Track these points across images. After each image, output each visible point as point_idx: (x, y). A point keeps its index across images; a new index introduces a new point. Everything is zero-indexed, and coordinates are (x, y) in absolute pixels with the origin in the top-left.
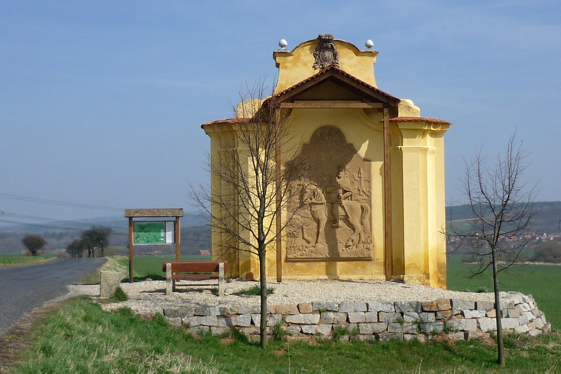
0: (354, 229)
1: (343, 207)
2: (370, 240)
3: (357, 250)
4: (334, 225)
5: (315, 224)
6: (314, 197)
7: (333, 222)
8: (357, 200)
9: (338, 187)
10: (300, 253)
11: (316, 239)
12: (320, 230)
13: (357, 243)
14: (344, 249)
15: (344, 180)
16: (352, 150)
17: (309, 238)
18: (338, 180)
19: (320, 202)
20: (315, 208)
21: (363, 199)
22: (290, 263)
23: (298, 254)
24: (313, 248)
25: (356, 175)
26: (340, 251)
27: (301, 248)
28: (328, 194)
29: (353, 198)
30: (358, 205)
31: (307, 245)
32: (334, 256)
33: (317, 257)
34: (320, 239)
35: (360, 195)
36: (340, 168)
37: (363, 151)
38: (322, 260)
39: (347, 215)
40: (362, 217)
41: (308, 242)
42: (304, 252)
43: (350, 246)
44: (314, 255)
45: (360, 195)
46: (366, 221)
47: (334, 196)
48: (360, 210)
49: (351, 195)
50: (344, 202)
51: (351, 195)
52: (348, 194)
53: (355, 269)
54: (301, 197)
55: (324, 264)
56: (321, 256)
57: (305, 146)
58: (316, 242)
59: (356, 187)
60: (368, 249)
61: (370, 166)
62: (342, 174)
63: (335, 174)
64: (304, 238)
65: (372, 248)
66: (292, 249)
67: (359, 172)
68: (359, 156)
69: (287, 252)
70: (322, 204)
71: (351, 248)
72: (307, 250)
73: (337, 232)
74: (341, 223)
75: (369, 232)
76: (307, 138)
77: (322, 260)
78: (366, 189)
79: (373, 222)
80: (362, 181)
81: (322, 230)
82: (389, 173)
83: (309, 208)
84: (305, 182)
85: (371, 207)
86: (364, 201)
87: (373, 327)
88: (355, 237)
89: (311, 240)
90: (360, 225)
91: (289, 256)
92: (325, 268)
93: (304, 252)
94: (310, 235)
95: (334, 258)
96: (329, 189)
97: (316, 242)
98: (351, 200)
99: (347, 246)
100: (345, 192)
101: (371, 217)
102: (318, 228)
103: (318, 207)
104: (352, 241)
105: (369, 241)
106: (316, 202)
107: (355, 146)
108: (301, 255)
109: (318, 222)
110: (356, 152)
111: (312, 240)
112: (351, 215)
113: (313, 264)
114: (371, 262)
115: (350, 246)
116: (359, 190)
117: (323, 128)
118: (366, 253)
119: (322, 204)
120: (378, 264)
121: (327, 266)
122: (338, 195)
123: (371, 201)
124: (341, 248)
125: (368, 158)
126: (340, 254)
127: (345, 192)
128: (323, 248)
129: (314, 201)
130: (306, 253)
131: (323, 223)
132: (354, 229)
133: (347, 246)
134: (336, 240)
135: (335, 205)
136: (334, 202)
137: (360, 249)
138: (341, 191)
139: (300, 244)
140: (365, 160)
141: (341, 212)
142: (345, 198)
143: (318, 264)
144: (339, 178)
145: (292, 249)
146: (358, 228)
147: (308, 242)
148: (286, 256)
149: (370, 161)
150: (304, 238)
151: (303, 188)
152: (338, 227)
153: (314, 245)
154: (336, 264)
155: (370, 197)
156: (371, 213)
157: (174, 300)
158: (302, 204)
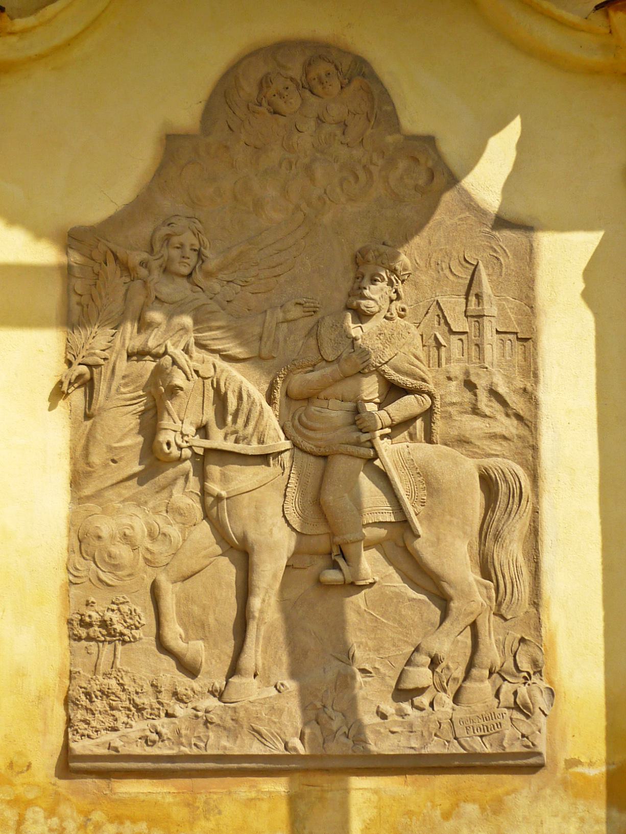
0: (443, 601)
1: (384, 479)
2: (530, 660)
3: (461, 713)
4: (332, 576)
5: (228, 571)
6: (222, 423)
7: (326, 556)
8: (462, 442)
9: (360, 363)
10: (139, 726)
11: (229, 648)
12: (256, 603)
13: (459, 673)
14: (389, 707)
15: (389, 330)
16: (434, 173)
17: (195, 649)
18: (355, 330)
19: (253, 448)
20: (225, 479)
21: (494, 437)
22: (91, 784)
23: (130, 736)
24: (212, 702)
25: (454, 306)
26: (369, 719)
27: (146, 700)
28: (297, 404)
29: (439, 426)
30: (463, 471)
31: (183, 682)
32: (334, 749)
33: (236, 751)
34: (253, 656)
35: (475, 411)
36: (368, 263)
37: (489, 177)
38: (268, 767)
39: (404, 523)
40: (488, 534)
41: (190, 669)
42: (162, 724)
43: (420, 691)
44: (218, 743)
45: (475, 411)
46: (511, 554)
47: (335, 413)
48: (478, 498)
49: (428, 415)
50: (389, 451)
51: (428, 415)
52: (408, 405)
53: (446, 816)
54: (150, 423)
55: (277, 786)
56: (256, 749)
57: (172, 144)
58: (234, 670)
59: (456, 369)
60: (523, 709)
61: (528, 258)
62: (376, 294)
63: (340, 298)
64: (163, 647)
65: (541, 701)
66: (100, 704)
67: (471, 289)
68: (470, 205)
69: (69, 722)
70: (264, 459)
71: (424, 700)
72: (180, 710)
73: (352, 617)
74: (371, 564)
75: (522, 605)
76: (186, 114)
77: (268, 767)
78: (509, 380)
79: (548, 560)
80: (489, 335)
81: (266, 604)
82: (512, 516)
83: (194, 483)
84: (172, 335)
85: (535, 478)
86: (496, 447)
87: (515, 693)
88: (450, 644)
89: (203, 657)
90: (473, 576)
91: (80, 746)
92: (283, 810)
93: (162, 724)
94: (196, 626)
95: (333, 755)
96: (299, 381)
97: (234, 670)
98: (429, 439)
99: (403, 694)
100: (393, 391)
101: (535, 532)
102: (245, 591)
103: (245, 477)
104: (434, 662)
105: (525, 666)
106: (229, 445)
107: (451, 149)
108: (146, 740)
109: (242, 554)
110: (453, 180)
111: (212, 657)
112: (429, 518)
113: (214, 789)
114: (541, 772)
115: (420, 691)
116: (470, 386)
117: (278, 50)
118: (508, 731)
119: (264, 459)
120: (574, 788)
121: (293, 800)
122: (357, 411)
123: (535, 449)
124: (372, 696)
125: (520, 211)
126: (370, 736)
127: (393, 391)
128: (271, 703)
129: (218, 440)
130: (175, 733)
131: (270, 571)
132: (443, 601)
133: (403, 694)
134: (349, 658)
135: (341, 465)
136: (331, 451)
137: (479, 708)
138: (371, 388)
139: (145, 676)
140: (501, 222)
141: (375, 505)
142: (399, 427)
143: (243, 788)
144: (362, 316)
145: (100, 704)
146: (467, 596)
147: (190, 669)
148: (66, 747)
149: (526, 227)
150: (163, 647)
151: (159, 372)
152: (353, 586)
153: (219, 683)
154: (346, 791)
155: (528, 422)
156: (536, 512)
157: (517, 533)
158: (154, 460)
